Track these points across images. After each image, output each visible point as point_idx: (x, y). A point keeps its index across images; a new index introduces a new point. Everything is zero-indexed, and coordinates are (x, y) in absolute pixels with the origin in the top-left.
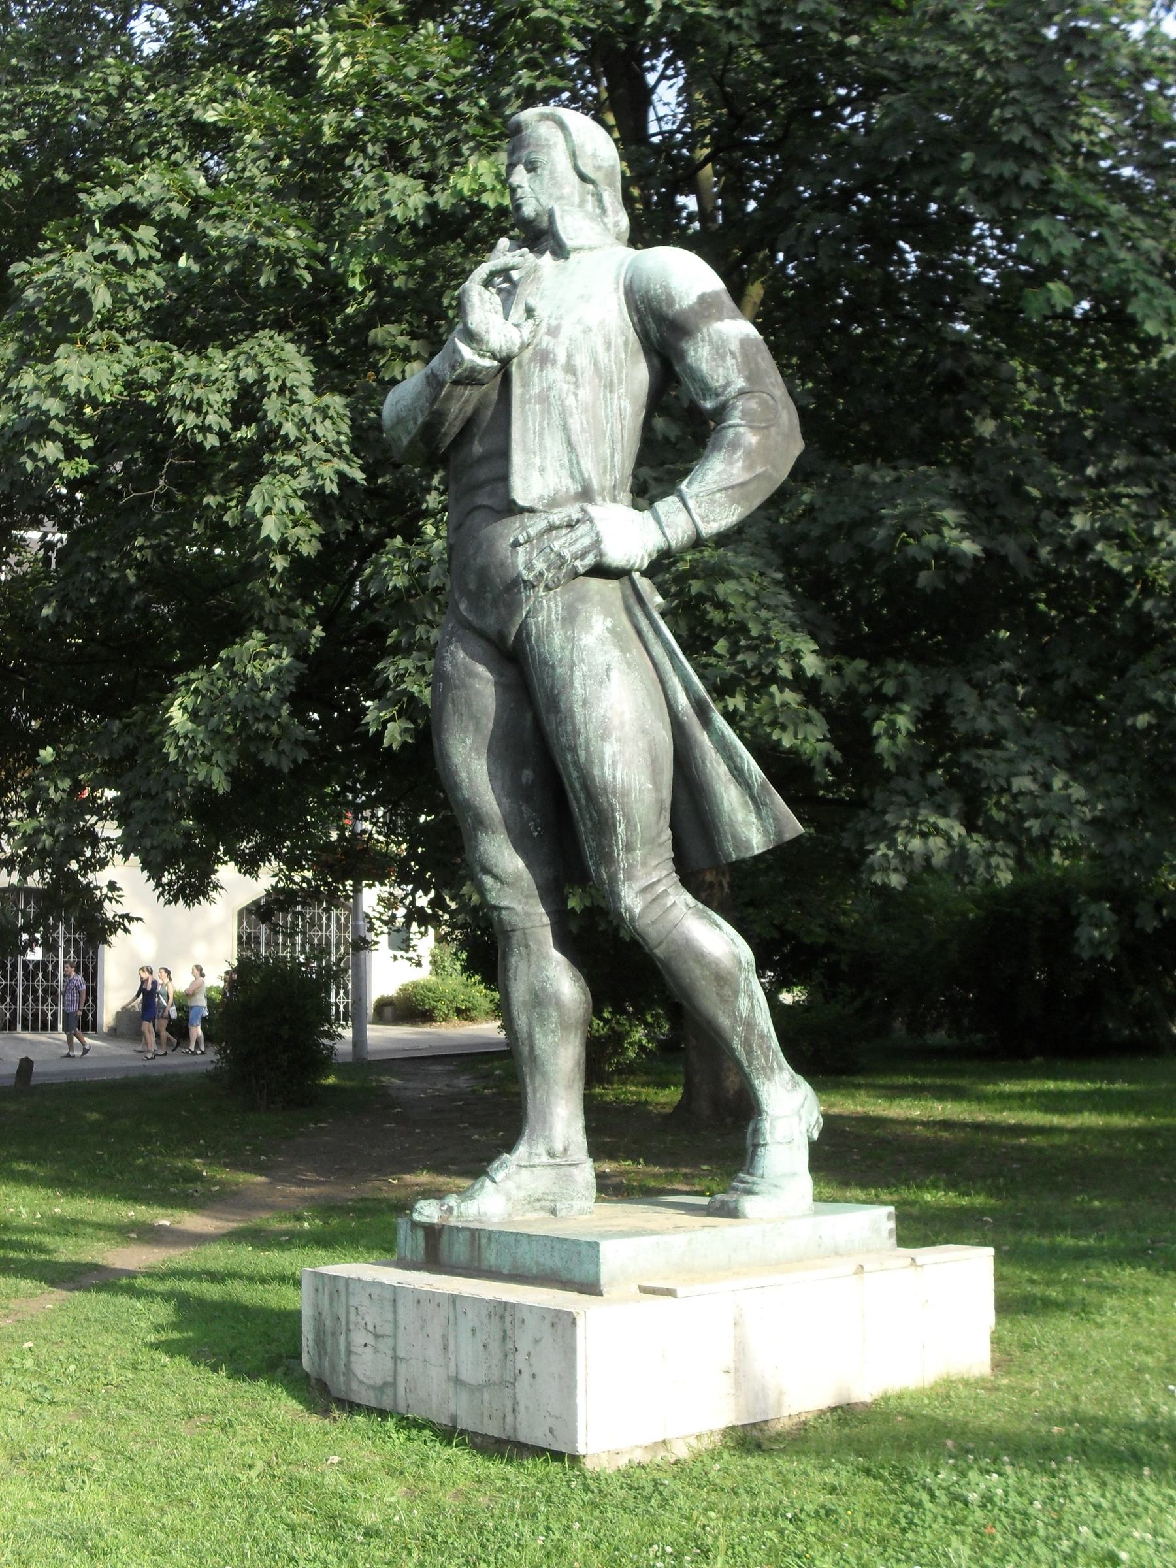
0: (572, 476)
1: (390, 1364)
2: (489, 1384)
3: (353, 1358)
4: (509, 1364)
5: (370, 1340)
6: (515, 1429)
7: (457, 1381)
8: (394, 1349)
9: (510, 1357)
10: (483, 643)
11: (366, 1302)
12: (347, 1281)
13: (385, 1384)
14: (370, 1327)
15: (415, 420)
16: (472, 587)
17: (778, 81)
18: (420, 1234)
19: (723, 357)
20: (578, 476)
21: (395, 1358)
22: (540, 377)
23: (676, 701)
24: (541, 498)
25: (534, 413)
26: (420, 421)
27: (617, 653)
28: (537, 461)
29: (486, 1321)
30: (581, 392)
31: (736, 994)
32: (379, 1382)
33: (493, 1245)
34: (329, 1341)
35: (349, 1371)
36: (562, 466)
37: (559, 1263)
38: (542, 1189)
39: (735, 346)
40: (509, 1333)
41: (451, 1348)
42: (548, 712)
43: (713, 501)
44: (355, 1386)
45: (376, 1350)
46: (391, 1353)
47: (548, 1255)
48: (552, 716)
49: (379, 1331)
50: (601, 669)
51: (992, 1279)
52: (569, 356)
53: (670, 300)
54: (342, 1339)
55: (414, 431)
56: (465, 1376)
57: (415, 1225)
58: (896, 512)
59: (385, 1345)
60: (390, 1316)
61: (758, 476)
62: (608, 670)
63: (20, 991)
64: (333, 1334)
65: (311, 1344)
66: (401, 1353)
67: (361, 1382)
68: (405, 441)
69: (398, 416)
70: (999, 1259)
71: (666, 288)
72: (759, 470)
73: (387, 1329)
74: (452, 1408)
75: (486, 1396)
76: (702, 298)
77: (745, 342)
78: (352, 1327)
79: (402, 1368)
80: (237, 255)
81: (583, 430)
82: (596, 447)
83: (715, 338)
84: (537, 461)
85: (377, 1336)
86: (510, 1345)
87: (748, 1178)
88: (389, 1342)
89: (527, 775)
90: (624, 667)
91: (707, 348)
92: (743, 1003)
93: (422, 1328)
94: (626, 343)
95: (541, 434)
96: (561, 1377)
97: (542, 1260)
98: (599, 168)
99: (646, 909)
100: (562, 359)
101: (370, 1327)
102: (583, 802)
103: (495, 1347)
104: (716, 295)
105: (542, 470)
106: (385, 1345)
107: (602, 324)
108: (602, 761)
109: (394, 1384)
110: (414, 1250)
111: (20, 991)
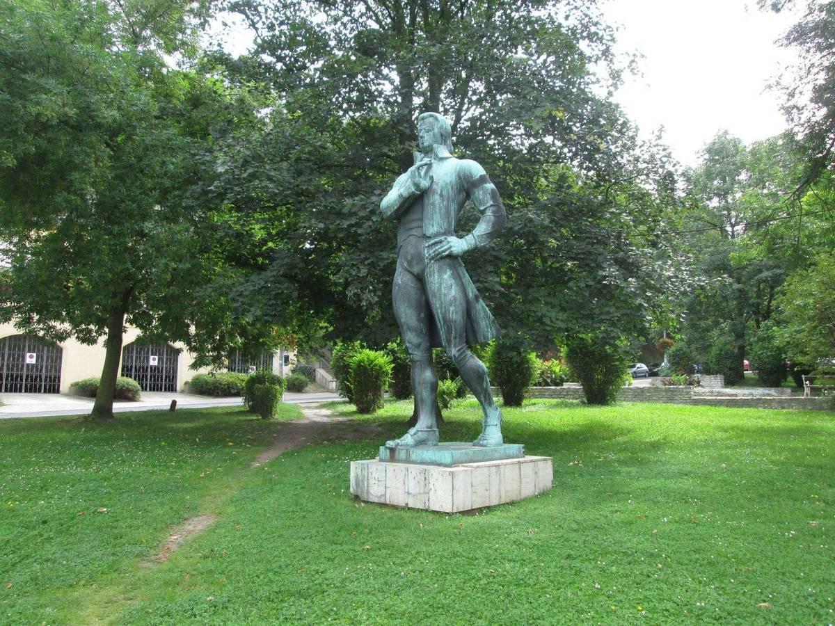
7: (408, 493)
17: (470, 59)
18: (388, 451)
32: (379, 495)
35: (368, 492)
39: (490, 191)
44: (371, 496)
51: (670, 406)
53: (472, 176)
54: (366, 483)
56: (410, 491)
57: (386, 448)
63: (134, 370)
68: (389, 214)
71: (470, 173)
73: (383, 479)
76: (481, 176)
77: (492, 190)
79: (388, 490)
80: (631, 334)
86: (427, 482)
87: (485, 442)
89: (422, 315)
100: (439, 192)
103: (422, 483)
104: (484, 176)
105: (433, 226)
109: (385, 495)
111: (134, 370)
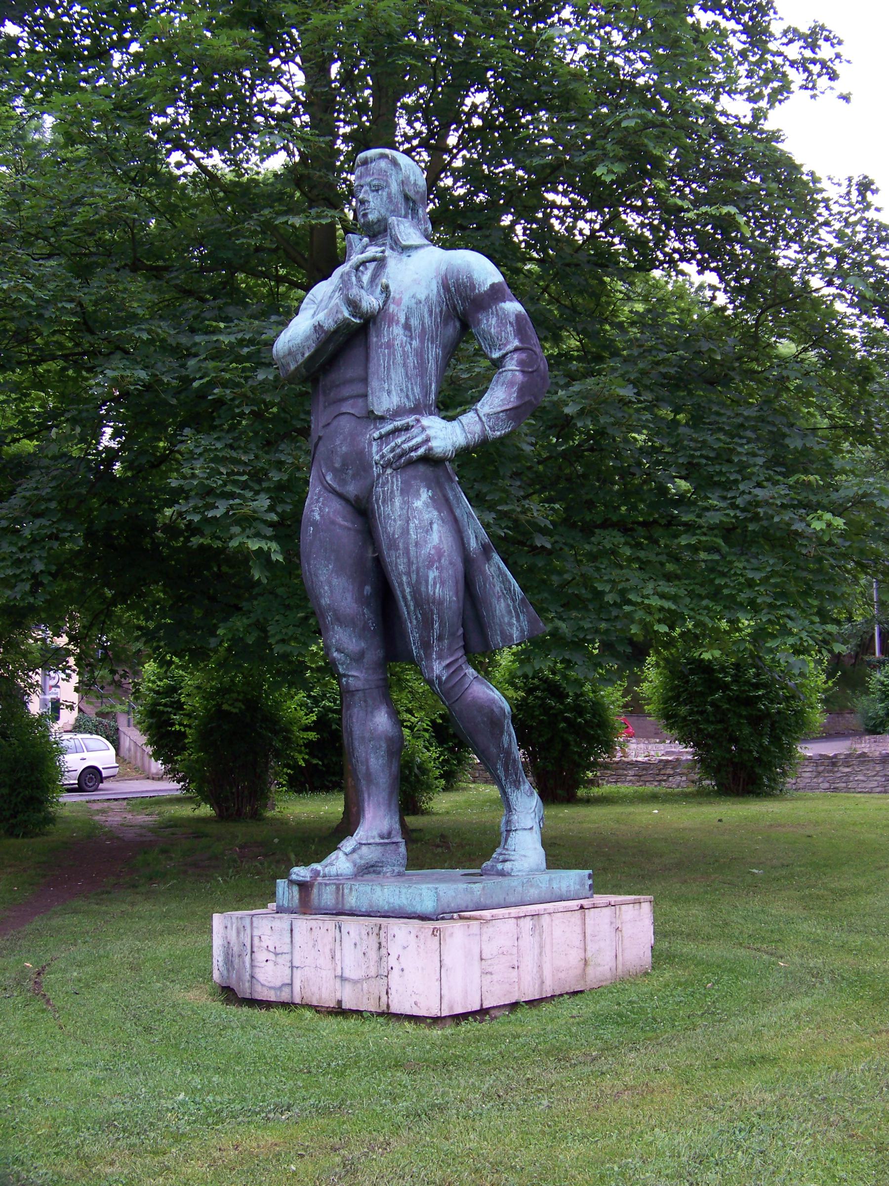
0: (407, 396)
1: (288, 971)
2: (368, 978)
3: (257, 970)
4: (384, 964)
5: (271, 957)
6: (388, 1006)
7: (343, 979)
8: (291, 961)
9: (384, 959)
10: (343, 503)
11: (269, 932)
12: (211, 931)
13: (284, 985)
14: (271, 948)
15: (303, 355)
16: (337, 465)
19: (505, 325)
20: (411, 397)
21: (292, 967)
22: (388, 331)
23: (469, 544)
24: (388, 410)
25: (384, 355)
26: (307, 355)
27: (436, 513)
28: (386, 386)
29: (365, 937)
30: (414, 342)
31: (502, 733)
32: (278, 984)
33: (354, 893)
34: (236, 960)
36: (401, 390)
37: (405, 902)
38: (375, 859)
39: (512, 319)
40: (383, 944)
41: (338, 956)
42: (389, 549)
43: (498, 418)
45: (276, 963)
46: (289, 964)
47: (396, 897)
48: (393, 553)
49: (278, 950)
50: (426, 523)
52: (407, 319)
53: (473, 287)
55: (301, 361)
56: (346, 974)
57: (292, 882)
58: (39, 294)
59: (284, 960)
60: (288, 940)
61: (525, 404)
62: (431, 524)
64: (239, 956)
65: (221, 964)
66: (296, 964)
67: (263, 985)
68: (293, 367)
69: (290, 349)
70: (655, 904)
71: (470, 278)
72: (527, 399)
73: (286, 948)
74: (338, 997)
75: (365, 985)
76: (493, 286)
77: (518, 316)
78: (255, 949)
79: (298, 974)
81: (415, 367)
82: (422, 378)
83: (500, 313)
84: (386, 386)
85: (276, 954)
86: (383, 951)
88: (288, 957)
89: (368, 589)
90: (440, 522)
91: (495, 319)
92: (505, 738)
93: (314, 946)
94: (441, 312)
95: (389, 369)
96: (423, 969)
97: (392, 901)
98: (418, 193)
99: (449, 678)
100: (402, 320)
101: (272, 949)
102: (412, 608)
104: (499, 284)
105: (389, 392)
106: (284, 960)
107: (427, 298)
108: (427, 581)
109: (291, 985)
110: (291, 900)
